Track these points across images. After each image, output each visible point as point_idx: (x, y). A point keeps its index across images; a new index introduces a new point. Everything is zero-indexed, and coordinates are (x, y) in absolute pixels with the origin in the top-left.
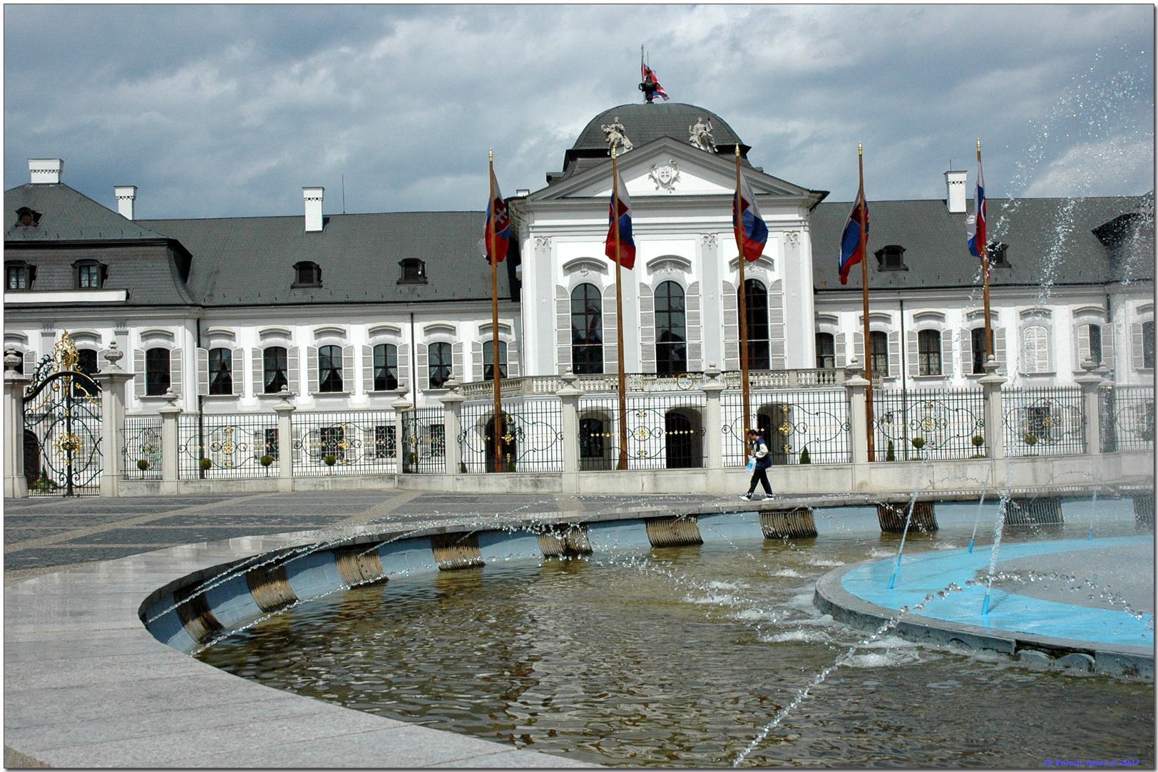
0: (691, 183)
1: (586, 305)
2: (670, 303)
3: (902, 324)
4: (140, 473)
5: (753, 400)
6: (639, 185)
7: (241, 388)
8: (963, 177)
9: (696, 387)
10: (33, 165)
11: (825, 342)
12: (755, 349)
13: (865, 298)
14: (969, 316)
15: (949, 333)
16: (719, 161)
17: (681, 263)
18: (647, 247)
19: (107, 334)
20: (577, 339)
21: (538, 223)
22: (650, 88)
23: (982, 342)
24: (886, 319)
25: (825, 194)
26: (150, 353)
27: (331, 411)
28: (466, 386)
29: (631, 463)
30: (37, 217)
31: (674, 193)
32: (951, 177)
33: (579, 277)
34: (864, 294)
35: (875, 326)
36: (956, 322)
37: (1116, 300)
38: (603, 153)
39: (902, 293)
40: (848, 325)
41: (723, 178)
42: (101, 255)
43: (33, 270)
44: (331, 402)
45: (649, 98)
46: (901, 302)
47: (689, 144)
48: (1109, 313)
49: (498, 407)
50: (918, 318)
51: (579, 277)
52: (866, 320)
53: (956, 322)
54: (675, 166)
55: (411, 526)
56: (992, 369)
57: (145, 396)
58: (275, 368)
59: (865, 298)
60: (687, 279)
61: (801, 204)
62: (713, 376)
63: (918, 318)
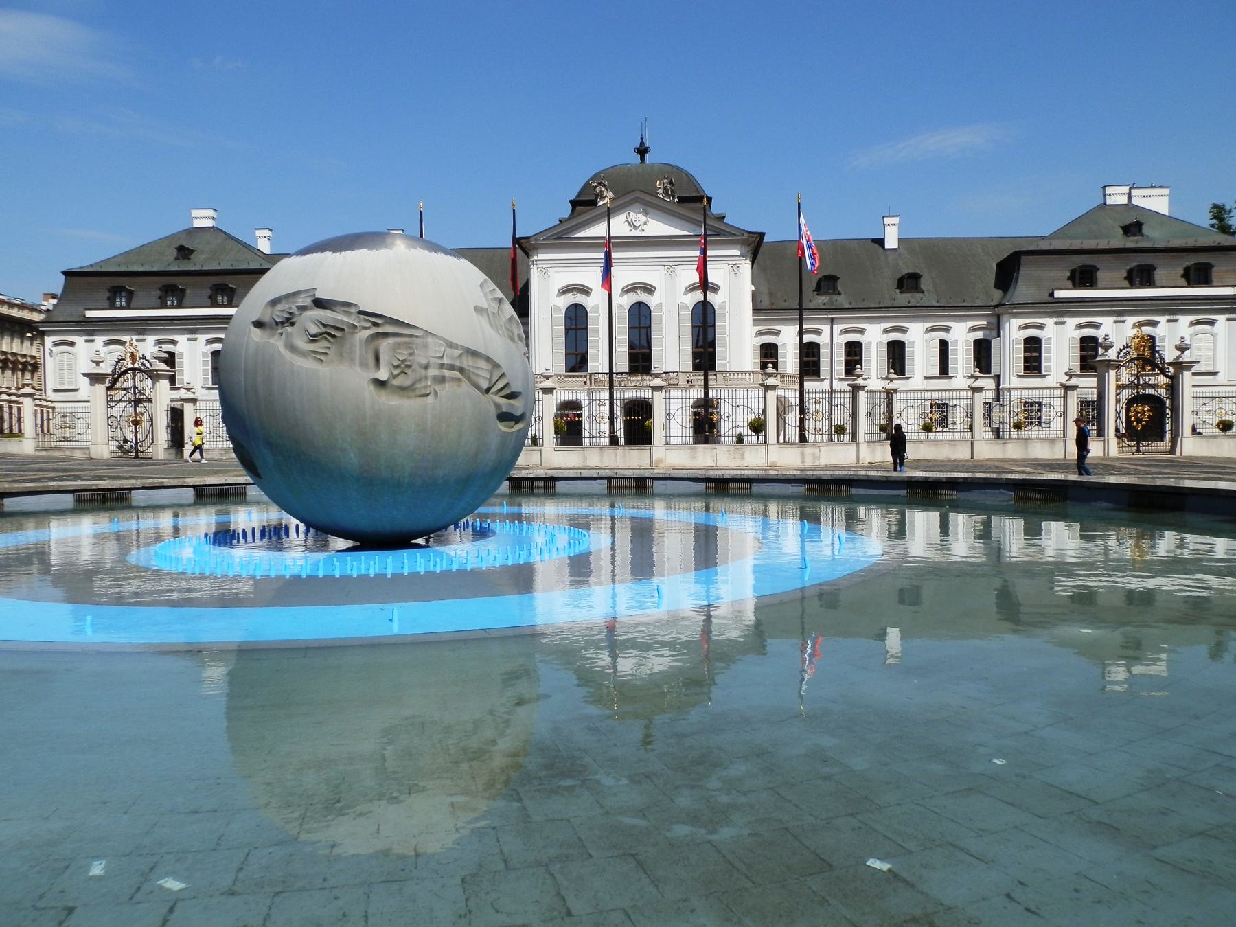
0: (656, 227)
1: (576, 320)
2: (640, 318)
3: (831, 337)
4: (924, 435)
5: (617, 394)
6: (620, 226)
7: (912, 371)
8: (896, 220)
9: (645, 383)
10: (195, 213)
11: (769, 353)
12: (704, 357)
13: (801, 316)
14: (972, 330)
15: (182, 354)
16: (681, 210)
17: (649, 289)
18: (622, 276)
19: (182, 339)
20: (631, 347)
21: (540, 256)
22: (642, 151)
23: (897, 355)
24: (819, 332)
25: (762, 235)
26: (1084, 340)
27: (944, 390)
28: (784, 375)
29: (809, 438)
30: (191, 252)
31: (644, 234)
32: (887, 220)
33: (570, 299)
34: (801, 311)
35: (807, 338)
36: (875, 337)
37: (1004, 318)
38: (593, 203)
39: (832, 313)
40: (788, 338)
41: (676, 220)
42: (127, 283)
43: (183, 291)
44: (943, 383)
45: (643, 159)
46: (832, 319)
47: (655, 195)
48: (997, 329)
49: (706, 393)
50: (844, 332)
51: (570, 299)
52: (801, 333)
53: (875, 337)
54: (646, 213)
55: (16, 485)
56: (860, 376)
57: (210, 385)
58: (897, 355)
59: (801, 316)
60: (652, 301)
61: (743, 243)
62: (547, 377)
63: (844, 332)
